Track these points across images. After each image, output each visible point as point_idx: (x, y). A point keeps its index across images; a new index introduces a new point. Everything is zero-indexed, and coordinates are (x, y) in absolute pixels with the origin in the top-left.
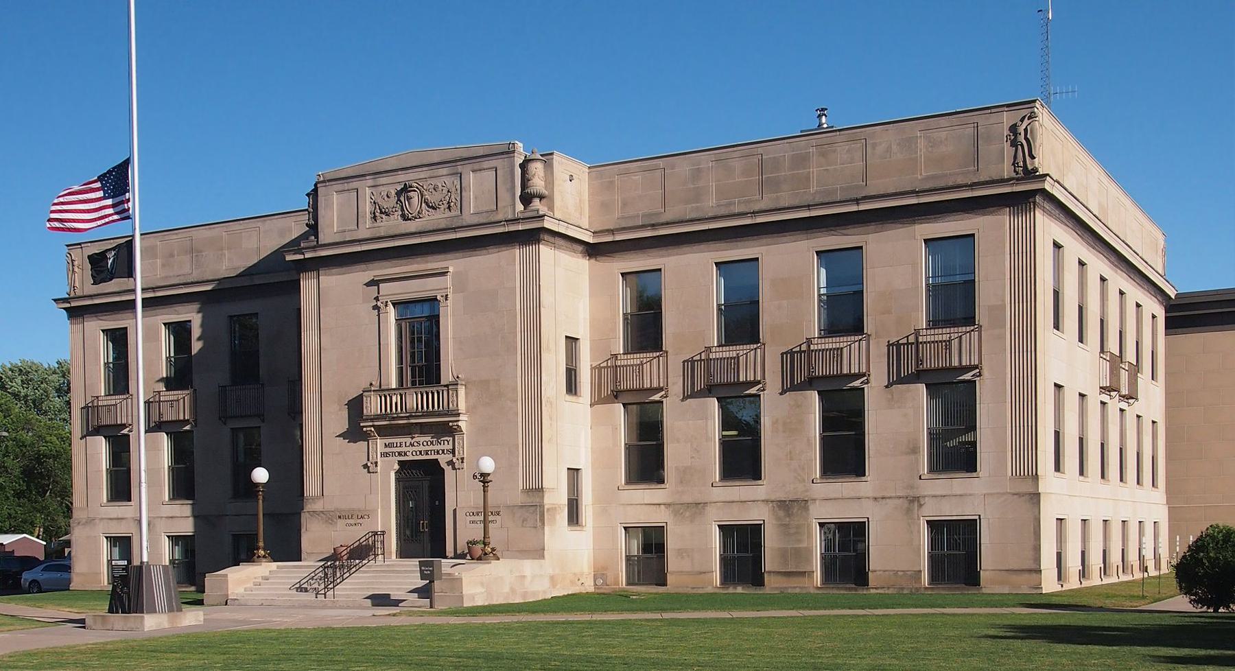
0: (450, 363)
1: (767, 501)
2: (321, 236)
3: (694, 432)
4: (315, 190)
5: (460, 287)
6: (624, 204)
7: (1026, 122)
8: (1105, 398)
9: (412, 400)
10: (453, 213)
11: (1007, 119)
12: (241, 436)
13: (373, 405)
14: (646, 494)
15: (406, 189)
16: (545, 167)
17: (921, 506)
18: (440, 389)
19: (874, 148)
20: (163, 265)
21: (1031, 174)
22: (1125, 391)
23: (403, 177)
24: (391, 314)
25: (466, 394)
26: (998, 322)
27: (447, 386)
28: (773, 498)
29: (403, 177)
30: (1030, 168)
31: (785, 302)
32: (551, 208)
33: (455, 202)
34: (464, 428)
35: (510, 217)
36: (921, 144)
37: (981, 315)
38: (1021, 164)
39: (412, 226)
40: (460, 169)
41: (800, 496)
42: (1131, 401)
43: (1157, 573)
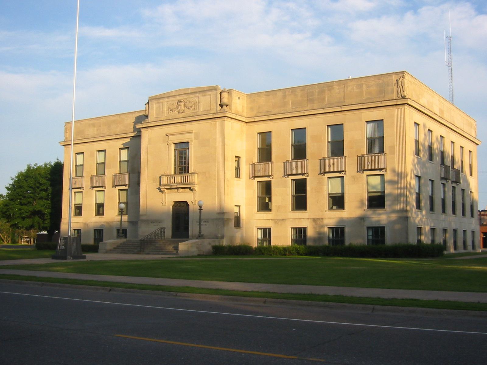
0: (193, 166)
1: (308, 219)
2: (149, 119)
3: (283, 193)
4: (148, 103)
5: (197, 137)
6: (259, 108)
7: (402, 78)
8: (444, 182)
9: (178, 179)
10: (195, 111)
11: (394, 78)
12: (297, 229)
13: (165, 181)
14: (264, 215)
15: (179, 102)
16: (228, 94)
17: (364, 221)
18: (188, 175)
19: (347, 88)
20: (97, 130)
21: (404, 97)
22: (453, 179)
23: (178, 98)
24: (173, 146)
25: (198, 177)
26: (393, 153)
27: (191, 174)
28: (311, 217)
29: (178, 98)
30: (403, 96)
31: (316, 144)
32: (231, 109)
33: (196, 105)
34: (196, 189)
35: (215, 112)
36: (364, 87)
37: (386, 150)
38: (400, 94)
39: (181, 115)
40: (198, 95)
41: (320, 217)
42: (458, 183)
43: (127, 186)
